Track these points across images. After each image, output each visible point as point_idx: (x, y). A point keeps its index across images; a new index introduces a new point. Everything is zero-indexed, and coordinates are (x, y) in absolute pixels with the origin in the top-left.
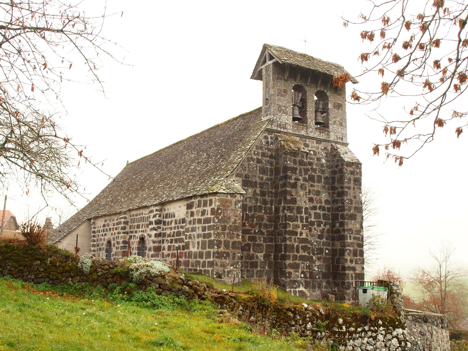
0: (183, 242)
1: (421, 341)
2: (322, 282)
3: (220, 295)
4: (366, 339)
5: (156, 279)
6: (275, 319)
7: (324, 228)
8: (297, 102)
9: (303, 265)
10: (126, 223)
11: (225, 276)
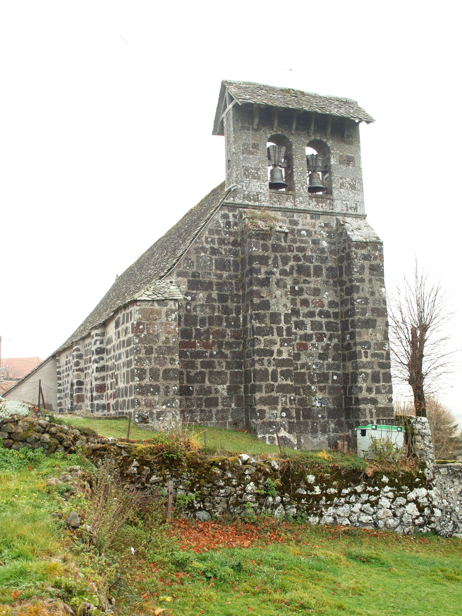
2: (328, 423)
5: (5, 425)
7: (329, 342)
9: (284, 399)
10: (80, 356)
11: (153, 420)
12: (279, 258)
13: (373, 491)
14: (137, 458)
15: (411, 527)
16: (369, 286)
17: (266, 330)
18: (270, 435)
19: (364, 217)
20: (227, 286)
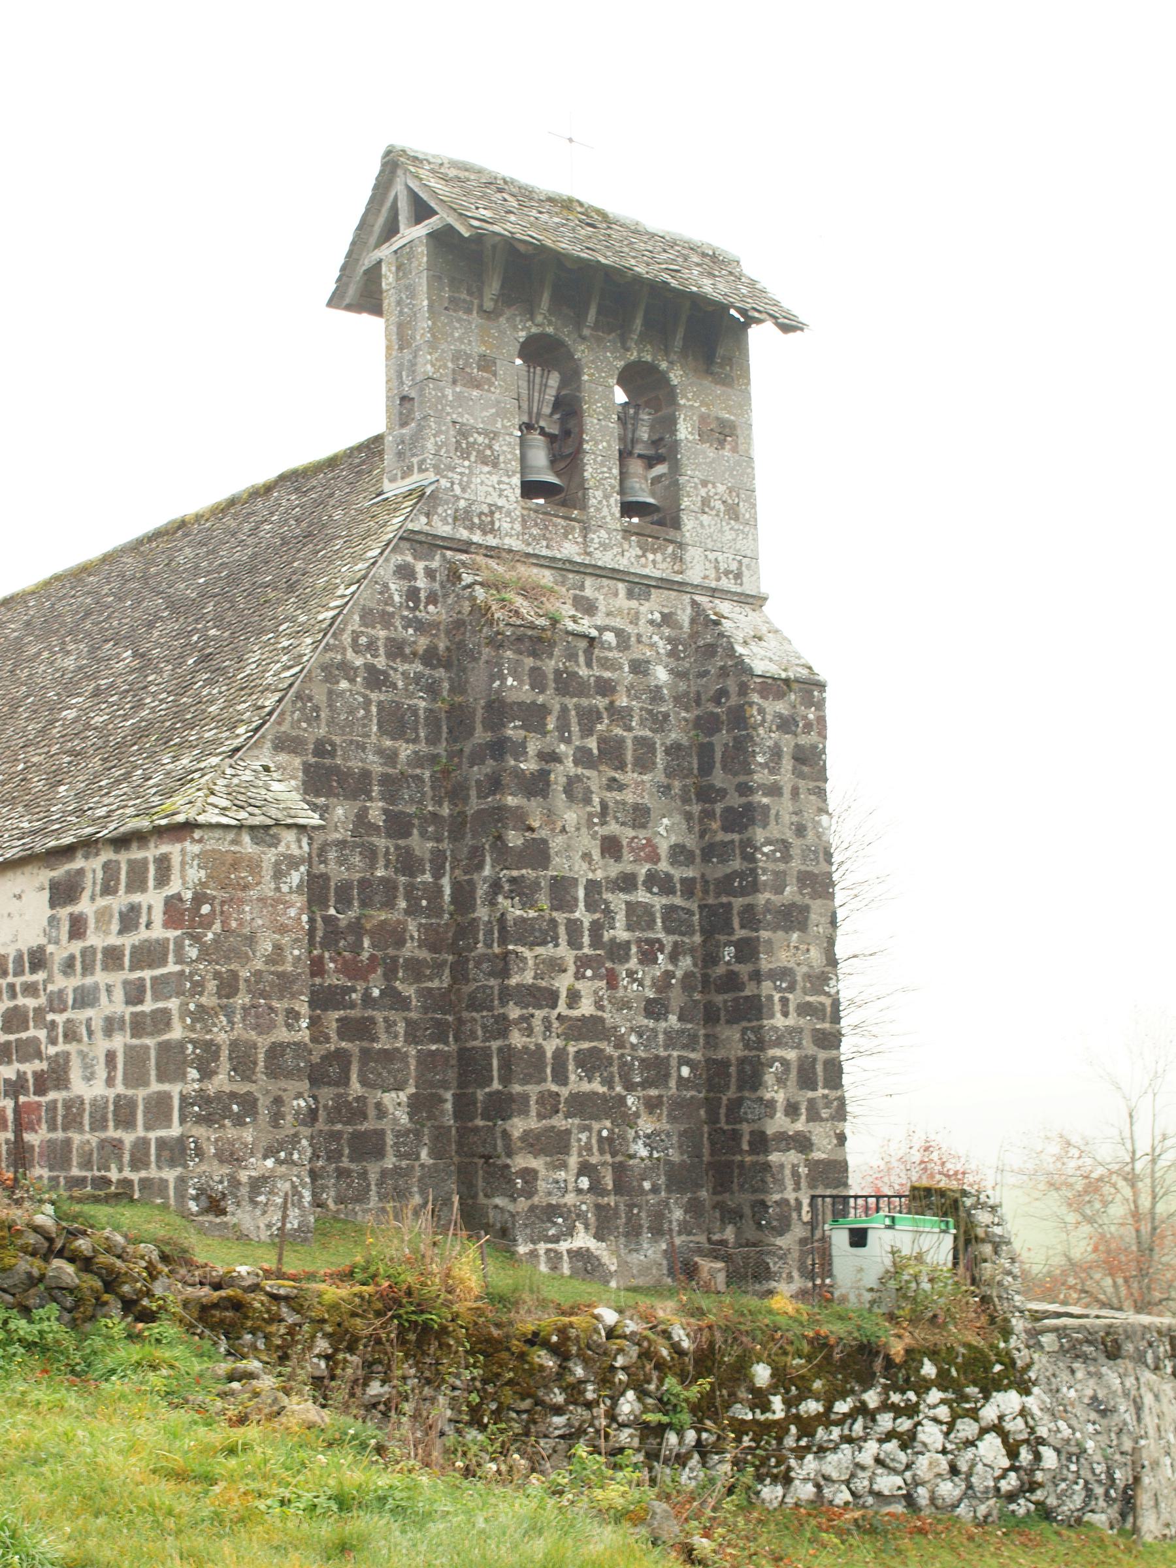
0: (39, 1055)
1: (1099, 1438)
2: (667, 1204)
3: (223, 1293)
4: (871, 1447)
6: (478, 1384)
7: (670, 968)
8: (539, 414)
11: (238, 1205)
12: (573, 713)
13: (902, 1404)
14: (328, 1329)
15: (992, 1502)
16: (791, 809)
17: (540, 929)
18: (550, 1246)
19: (759, 602)
20: (408, 787)
